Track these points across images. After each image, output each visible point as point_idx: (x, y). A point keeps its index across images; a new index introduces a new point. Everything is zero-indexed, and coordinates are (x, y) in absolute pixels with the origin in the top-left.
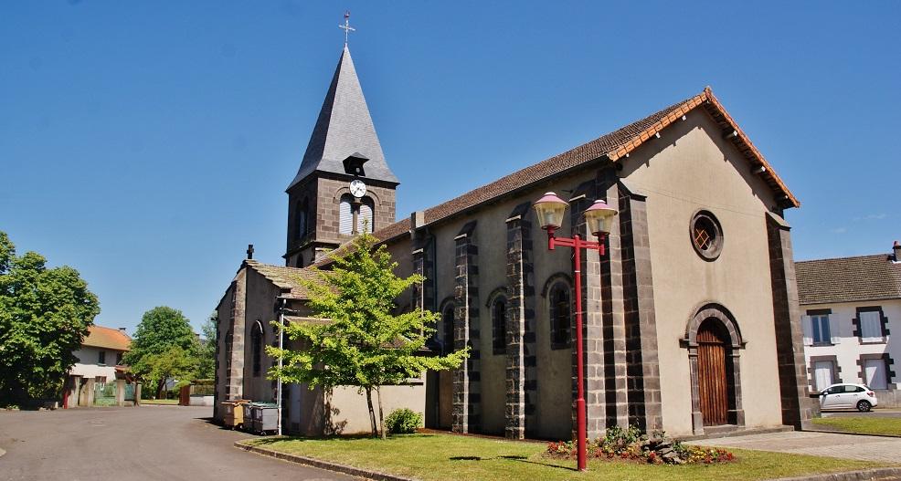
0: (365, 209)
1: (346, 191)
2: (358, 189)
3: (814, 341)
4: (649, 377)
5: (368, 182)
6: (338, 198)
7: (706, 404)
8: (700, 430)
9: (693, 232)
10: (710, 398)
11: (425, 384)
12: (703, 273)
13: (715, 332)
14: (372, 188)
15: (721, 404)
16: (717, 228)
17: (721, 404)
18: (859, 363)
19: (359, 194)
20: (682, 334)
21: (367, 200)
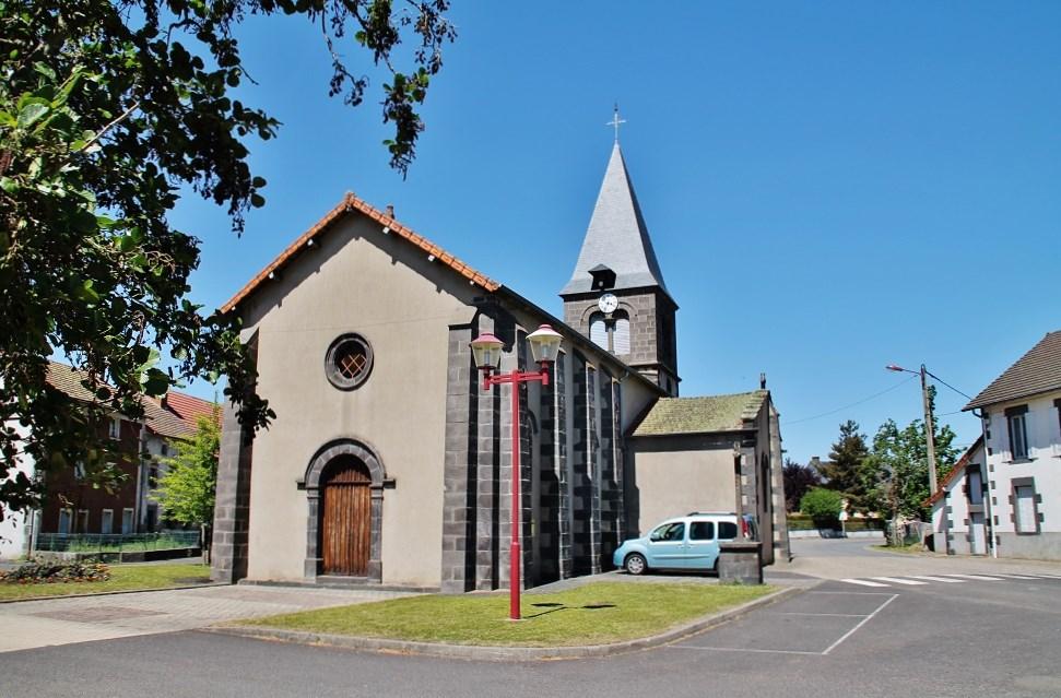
0: (621, 323)
1: (594, 309)
2: (608, 304)
3: (1013, 457)
4: (222, 519)
5: (619, 293)
6: (586, 319)
7: (343, 551)
8: (313, 578)
9: (363, 344)
10: (350, 545)
11: (478, 546)
12: (339, 405)
13: (343, 471)
14: (623, 299)
15: (343, 551)
16: (360, 341)
17: (343, 551)
18: (1041, 515)
19: (610, 309)
20: (301, 475)
21: (620, 314)
